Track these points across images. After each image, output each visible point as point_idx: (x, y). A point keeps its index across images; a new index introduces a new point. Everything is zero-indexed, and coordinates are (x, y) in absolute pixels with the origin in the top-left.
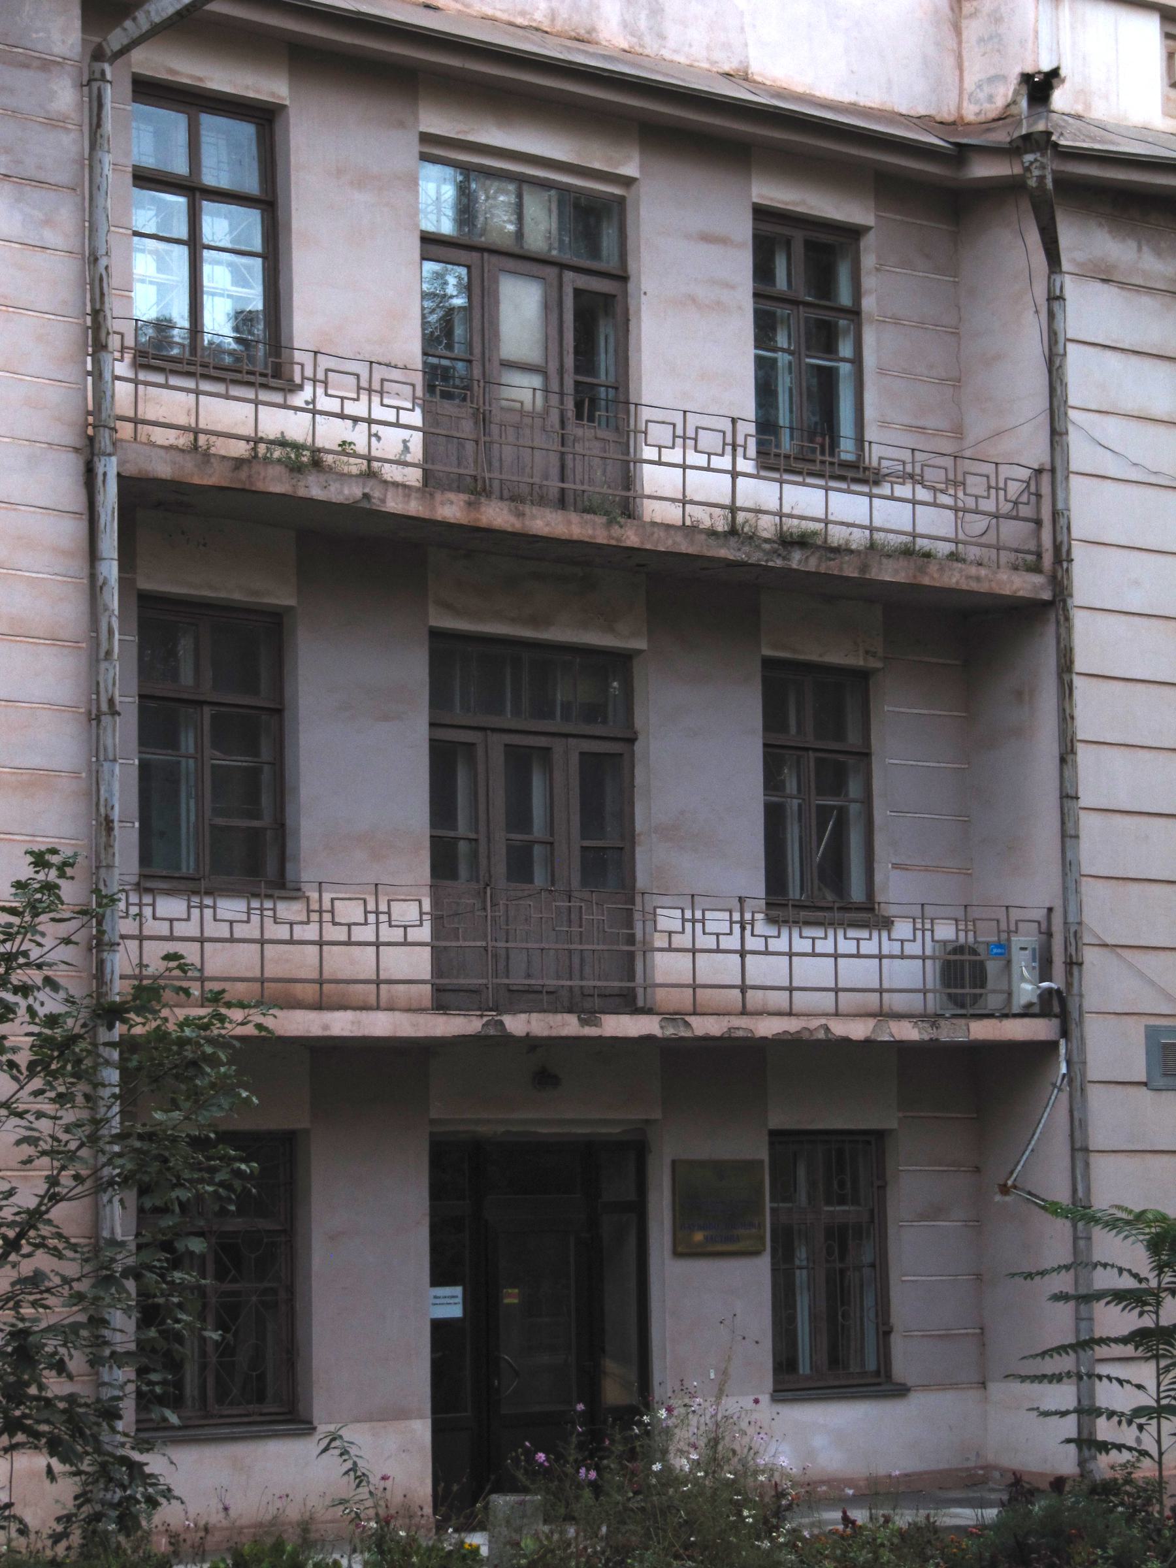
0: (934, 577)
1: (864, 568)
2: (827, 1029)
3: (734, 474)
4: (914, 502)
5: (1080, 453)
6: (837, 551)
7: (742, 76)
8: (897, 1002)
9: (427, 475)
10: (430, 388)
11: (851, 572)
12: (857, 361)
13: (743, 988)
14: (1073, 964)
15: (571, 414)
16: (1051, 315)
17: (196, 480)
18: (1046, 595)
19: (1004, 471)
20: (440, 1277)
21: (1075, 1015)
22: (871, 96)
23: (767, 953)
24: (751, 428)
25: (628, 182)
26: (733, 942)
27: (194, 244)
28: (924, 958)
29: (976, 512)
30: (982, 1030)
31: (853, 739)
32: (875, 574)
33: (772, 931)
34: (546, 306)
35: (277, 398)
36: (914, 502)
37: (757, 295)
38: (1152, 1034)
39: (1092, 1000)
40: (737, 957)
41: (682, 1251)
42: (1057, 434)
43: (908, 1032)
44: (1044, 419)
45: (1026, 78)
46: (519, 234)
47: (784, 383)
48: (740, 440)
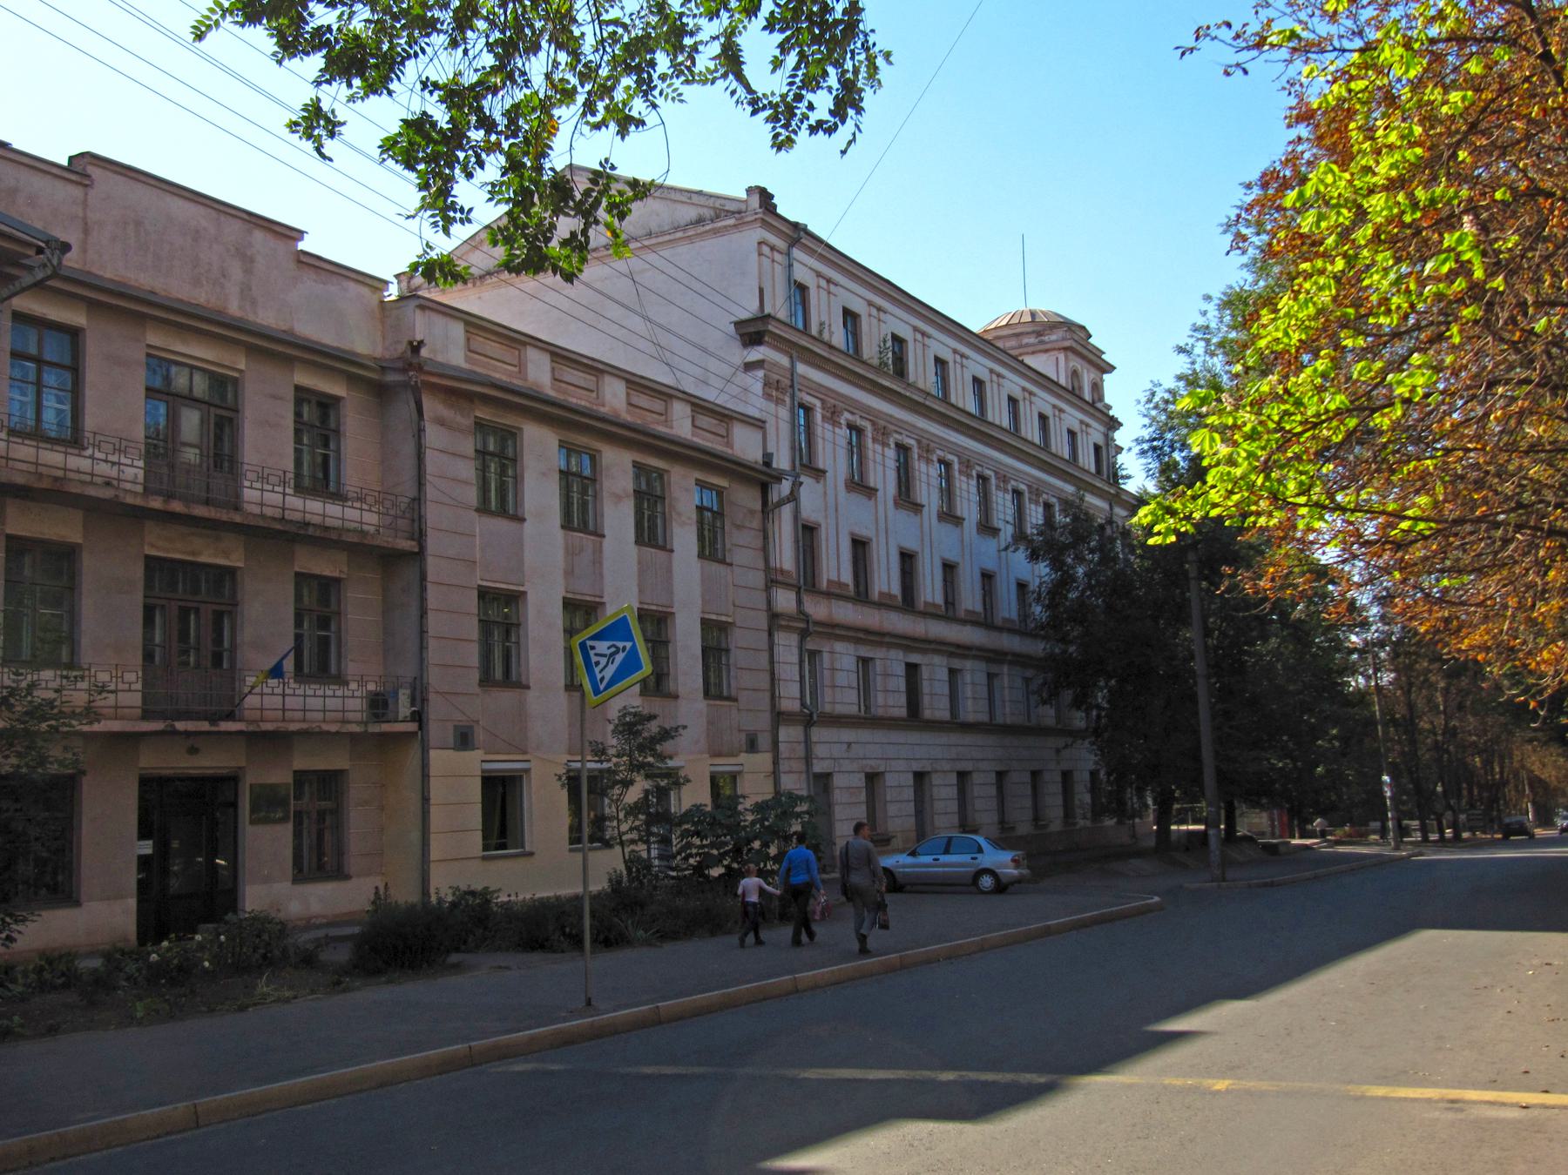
1: (340, 535)
3: (284, 494)
5: (430, 492)
9: (145, 489)
10: (147, 452)
12: (338, 451)
14: (424, 700)
15: (212, 466)
17: (35, 485)
18: (416, 550)
19: (400, 499)
20: (144, 834)
23: (294, 695)
24: (292, 476)
25: (241, 371)
27: (39, 385)
30: (386, 727)
31: (334, 607)
32: (344, 538)
33: (297, 686)
34: (202, 421)
35: (76, 452)
36: (361, 509)
37: (295, 421)
38: (455, 726)
39: (432, 716)
41: (252, 822)
45: (411, 343)
46: (191, 389)
47: (306, 458)
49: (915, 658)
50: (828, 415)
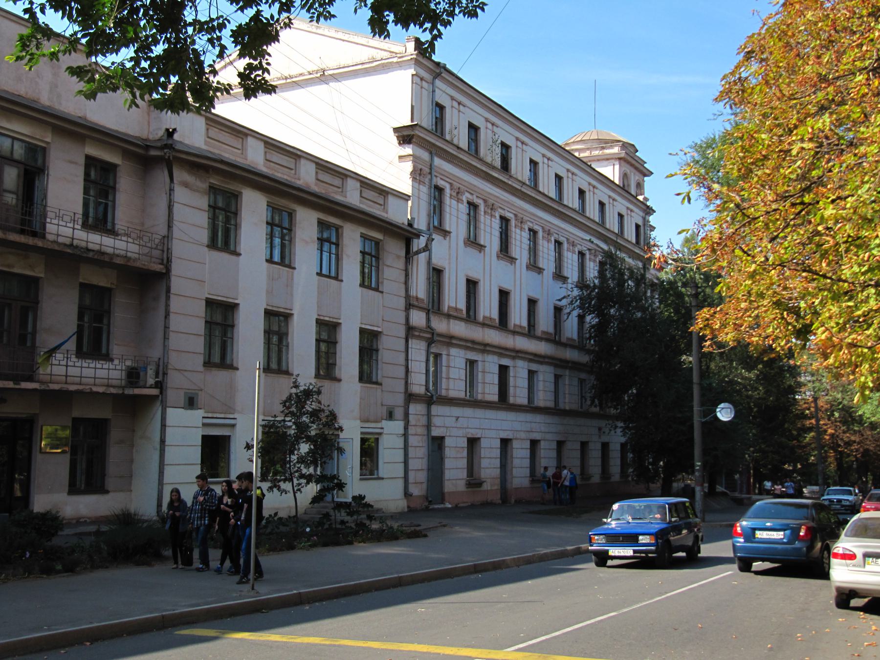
0: (131, 264)
1: (112, 259)
2: (91, 389)
4: (127, 242)
5: (176, 233)
6: (77, 247)
7: (85, 119)
8: (115, 382)
11: (107, 259)
13: (66, 376)
14: (165, 374)
16: (170, 195)
18: (164, 271)
19: (154, 236)
21: (164, 388)
22: (131, 132)
26: (64, 363)
28: (122, 370)
29: (146, 246)
30: (137, 391)
33: (76, 360)
36: (127, 242)
40: (65, 368)
42: (170, 227)
43: (113, 391)
44: (167, 223)
48: (76, 219)
49: (505, 362)
50: (454, 194)
